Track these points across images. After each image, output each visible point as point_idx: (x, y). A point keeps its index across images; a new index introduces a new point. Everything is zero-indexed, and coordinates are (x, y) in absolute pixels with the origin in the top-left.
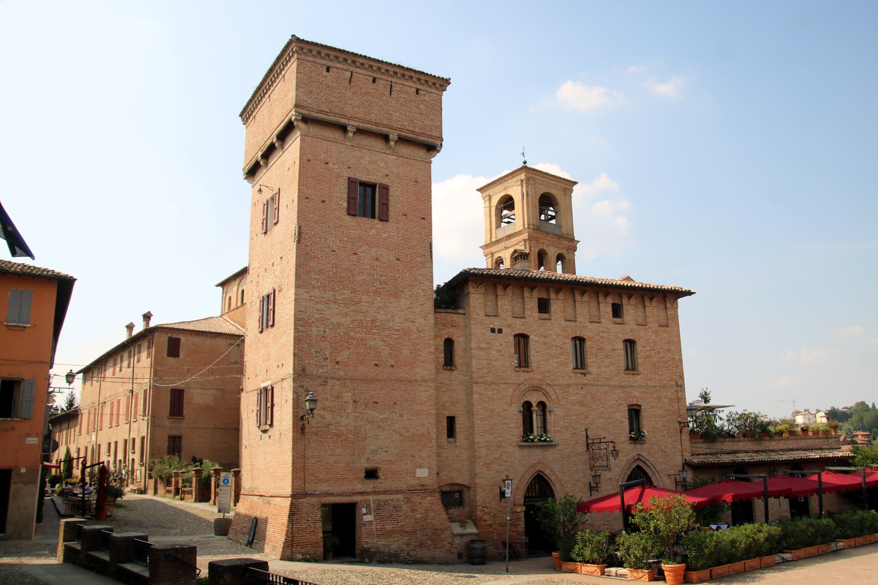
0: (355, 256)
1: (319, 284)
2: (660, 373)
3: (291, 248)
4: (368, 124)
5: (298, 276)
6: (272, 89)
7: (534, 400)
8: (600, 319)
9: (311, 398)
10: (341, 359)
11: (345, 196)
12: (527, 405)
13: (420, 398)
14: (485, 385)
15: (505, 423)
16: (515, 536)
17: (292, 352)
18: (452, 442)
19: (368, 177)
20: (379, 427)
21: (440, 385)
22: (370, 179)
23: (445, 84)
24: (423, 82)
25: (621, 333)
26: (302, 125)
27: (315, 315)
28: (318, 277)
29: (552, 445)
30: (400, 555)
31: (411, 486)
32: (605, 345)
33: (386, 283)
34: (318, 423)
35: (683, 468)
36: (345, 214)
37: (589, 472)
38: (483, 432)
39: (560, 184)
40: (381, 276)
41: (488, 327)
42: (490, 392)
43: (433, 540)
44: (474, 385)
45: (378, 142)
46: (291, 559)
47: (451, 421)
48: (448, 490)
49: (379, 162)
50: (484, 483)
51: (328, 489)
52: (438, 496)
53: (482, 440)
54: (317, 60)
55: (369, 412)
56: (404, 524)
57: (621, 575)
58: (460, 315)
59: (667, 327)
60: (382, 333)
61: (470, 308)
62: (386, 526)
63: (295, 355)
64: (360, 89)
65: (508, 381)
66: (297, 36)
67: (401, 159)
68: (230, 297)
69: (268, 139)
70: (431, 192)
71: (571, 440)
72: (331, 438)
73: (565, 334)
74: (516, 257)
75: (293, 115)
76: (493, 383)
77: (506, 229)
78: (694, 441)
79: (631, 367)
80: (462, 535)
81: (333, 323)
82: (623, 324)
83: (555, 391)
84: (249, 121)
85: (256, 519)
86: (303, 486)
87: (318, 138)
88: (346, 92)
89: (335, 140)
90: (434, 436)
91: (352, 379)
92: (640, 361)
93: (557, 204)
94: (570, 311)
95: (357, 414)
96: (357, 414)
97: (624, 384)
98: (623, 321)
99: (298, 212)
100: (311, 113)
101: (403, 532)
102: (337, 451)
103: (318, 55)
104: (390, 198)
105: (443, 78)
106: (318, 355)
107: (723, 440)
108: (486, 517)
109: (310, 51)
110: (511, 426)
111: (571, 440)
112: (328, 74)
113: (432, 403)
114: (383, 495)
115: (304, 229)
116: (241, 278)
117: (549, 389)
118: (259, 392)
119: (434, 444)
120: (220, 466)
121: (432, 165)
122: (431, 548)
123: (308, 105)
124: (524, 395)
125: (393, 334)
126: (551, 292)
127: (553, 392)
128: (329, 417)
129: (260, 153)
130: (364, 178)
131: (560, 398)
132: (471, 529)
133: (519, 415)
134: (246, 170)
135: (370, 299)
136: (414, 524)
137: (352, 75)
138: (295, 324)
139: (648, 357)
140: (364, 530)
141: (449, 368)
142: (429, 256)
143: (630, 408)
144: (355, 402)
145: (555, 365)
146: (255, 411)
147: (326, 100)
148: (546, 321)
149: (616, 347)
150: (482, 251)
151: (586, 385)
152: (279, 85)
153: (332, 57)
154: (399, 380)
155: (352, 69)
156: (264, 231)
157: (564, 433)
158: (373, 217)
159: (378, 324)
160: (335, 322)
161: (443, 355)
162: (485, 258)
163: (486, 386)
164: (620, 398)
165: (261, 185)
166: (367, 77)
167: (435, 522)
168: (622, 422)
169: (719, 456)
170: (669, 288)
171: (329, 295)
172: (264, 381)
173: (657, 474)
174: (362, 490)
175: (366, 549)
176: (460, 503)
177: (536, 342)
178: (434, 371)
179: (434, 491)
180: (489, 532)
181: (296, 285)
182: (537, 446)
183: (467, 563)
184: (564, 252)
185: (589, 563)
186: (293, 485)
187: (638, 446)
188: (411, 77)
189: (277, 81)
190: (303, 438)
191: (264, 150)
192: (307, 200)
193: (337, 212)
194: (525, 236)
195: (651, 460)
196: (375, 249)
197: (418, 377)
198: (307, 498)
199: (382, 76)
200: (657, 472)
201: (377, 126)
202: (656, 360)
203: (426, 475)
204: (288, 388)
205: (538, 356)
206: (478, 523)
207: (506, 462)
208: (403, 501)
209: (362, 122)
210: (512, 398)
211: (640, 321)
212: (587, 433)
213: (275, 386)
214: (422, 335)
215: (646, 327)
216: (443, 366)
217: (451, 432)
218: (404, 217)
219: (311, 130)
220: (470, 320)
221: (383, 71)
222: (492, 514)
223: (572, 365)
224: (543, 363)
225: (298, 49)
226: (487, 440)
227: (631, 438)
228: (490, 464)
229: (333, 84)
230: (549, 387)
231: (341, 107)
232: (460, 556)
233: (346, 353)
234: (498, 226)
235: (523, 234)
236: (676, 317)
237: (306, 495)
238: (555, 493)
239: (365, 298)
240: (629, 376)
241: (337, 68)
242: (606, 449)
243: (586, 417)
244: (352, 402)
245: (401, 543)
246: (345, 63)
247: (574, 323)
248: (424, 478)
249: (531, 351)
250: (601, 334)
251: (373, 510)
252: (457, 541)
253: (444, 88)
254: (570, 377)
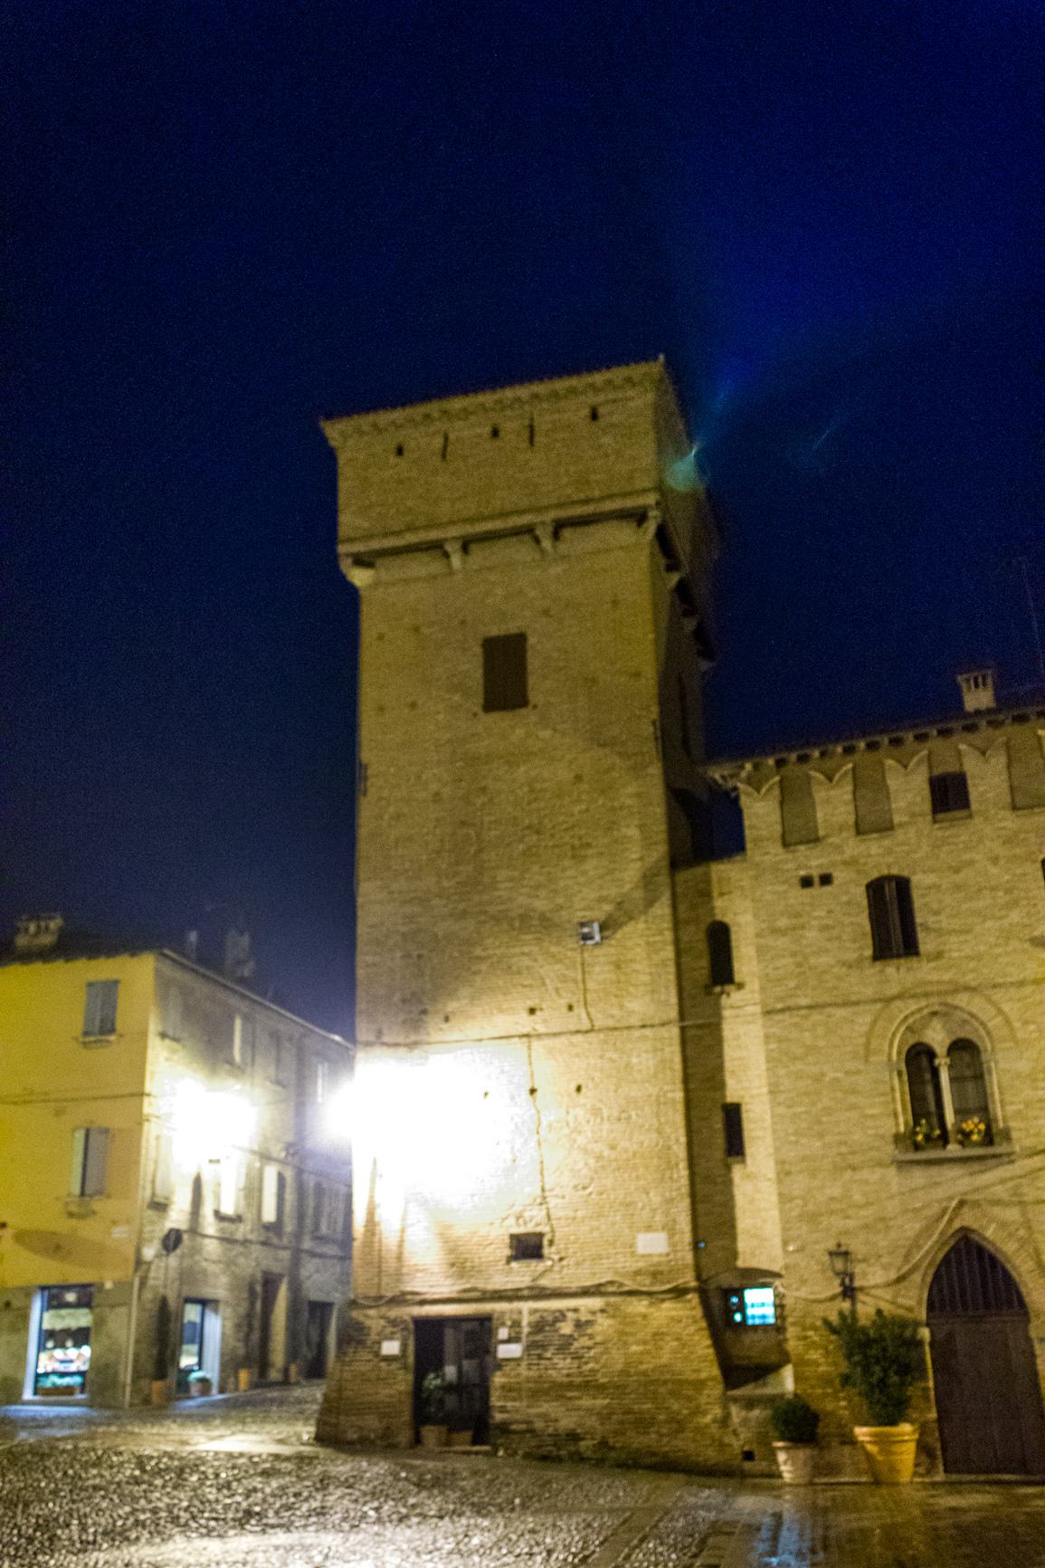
12: (919, 1060)
15: (853, 1107)
42: (807, 1034)
110: (869, 1112)
112: (398, 460)
127: (993, 1012)
131: (1017, 1025)
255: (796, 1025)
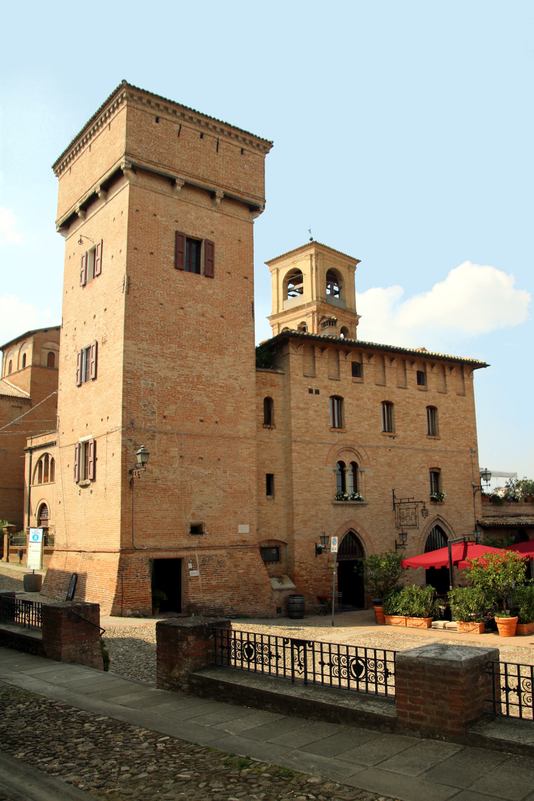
0: (181, 310)
1: (148, 336)
2: (458, 439)
3: (118, 299)
4: (196, 178)
5: (127, 328)
6: (93, 138)
7: (347, 460)
8: (406, 385)
9: (143, 452)
10: (168, 413)
11: (173, 249)
12: (342, 464)
13: (242, 455)
14: (303, 444)
15: (321, 482)
16: (329, 591)
17: (121, 404)
18: (270, 499)
19: (194, 232)
20: (204, 483)
21: (260, 443)
22: (196, 234)
23: (268, 147)
24: (248, 142)
25: (425, 400)
26: (131, 174)
27: (143, 368)
28: (147, 330)
29: (363, 504)
30: (224, 610)
31: (233, 542)
32: (411, 410)
33: (211, 340)
34: (146, 477)
35: (476, 529)
36: (173, 267)
37: (395, 530)
38: (301, 490)
39: (345, 261)
40: (207, 332)
41: (307, 388)
43: (254, 595)
44: (293, 443)
45: (204, 198)
46: (121, 615)
47: (270, 478)
48: (266, 546)
49: (205, 218)
50: (301, 539)
51: (155, 544)
52: (258, 551)
53: (300, 497)
54: (146, 109)
55: (195, 467)
56: (227, 579)
57: (449, 628)
58: (279, 375)
59: (464, 395)
60: (208, 389)
61: (289, 369)
62: (211, 582)
63: (123, 407)
64: (189, 143)
65: (324, 441)
66: (129, 82)
67: (226, 217)
68: (11, 361)
69: (89, 190)
70: (253, 252)
71: (380, 500)
72: (159, 493)
73: (375, 398)
74: (324, 323)
75: (122, 163)
76: (310, 442)
77: (292, 302)
78: (484, 504)
79: (433, 432)
80: (281, 590)
81: (161, 377)
82: (426, 391)
83: (366, 453)
84: (63, 173)
85: (75, 574)
86: (131, 541)
87: (146, 189)
88: (175, 144)
89: (163, 193)
90: (255, 493)
91: (178, 434)
92: (440, 427)
93: (342, 280)
94: (380, 376)
95: (184, 469)
96: (184, 469)
97: (426, 448)
98: (426, 388)
99: (127, 262)
100: (141, 162)
101: (227, 587)
102: (165, 506)
103: (148, 104)
104: (215, 255)
105: (266, 140)
106: (146, 408)
107: (508, 503)
108: (303, 573)
109: (140, 99)
110: (326, 484)
111: (380, 500)
112: (157, 124)
113: (253, 460)
114: (207, 551)
115: (133, 280)
116: (23, 342)
117: (361, 451)
118: (77, 446)
119: (254, 500)
120: (9, 523)
121: (254, 225)
122: (253, 603)
123: (138, 154)
124: (338, 455)
125: (218, 391)
126: (363, 356)
127: (364, 454)
128: (156, 472)
129: (78, 205)
130: (190, 233)
131: (371, 459)
132: (289, 585)
133: (333, 474)
134: (61, 222)
135: (196, 355)
136: (237, 579)
137: (180, 128)
138: (124, 376)
139: (447, 424)
140: (191, 585)
141: (269, 426)
142: (251, 315)
143: (431, 471)
144: (181, 457)
145: (367, 427)
146: (72, 466)
147: (155, 150)
148: (359, 385)
149: (420, 412)
150: (268, 321)
151: (393, 447)
152: (103, 134)
153: (161, 107)
154: (222, 436)
155: (181, 122)
156: (83, 283)
157: (374, 492)
158: (198, 272)
159: (204, 380)
160: (162, 376)
161: (263, 414)
162: (272, 328)
163: (304, 445)
164: (423, 461)
165: (81, 236)
166: (195, 131)
167: (256, 577)
168: (424, 484)
169: (505, 518)
170: (468, 359)
171: (157, 348)
172: (83, 436)
173: (453, 534)
174: (188, 546)
175: (193, 604)
176: (277, 559)
177: (349, 404)
178: (255, 429)
179: (254, 547)
180: (305, 587)
181: (125, 336)
182: (349, 504)
183: (285, 617)
184: (347, 325)
185: (416, 617)
186: (122, 540)
187: (438, 507)
188: (237, 137)
189: (101, 130)
190: (131, 492)
191: (84, 201)
192: (135, 251)
193: (165, 265)
194: (314, 308)
195: (449, 520)
196: (201, 305)
197: (241, 434)
198: (135, 554)
199: (209, 132)
200: (454, 532)
201: (205, 182)
202: (454, 426)
203: (247, 531)
204: (116, 442)
205: (351, 417)
206: (296, 578)
207: (321, 519)
208: (226, 556)
209: (190, 177)
210: (327, 458)
211: (441, 388)
212: (393, 493)
213: (97, 440)
214: (244, 393)
215: (446, 395)
216: (263, 424)
217: (270, 490)
218: (227, 274)
219: (140, 180)
220: (290, 380)
221: (210, 127)
222: (308, 570)
223: (382, 428)
224: (355, 425)
225: (128, 95)
226: (305, 498)
227: (433, 499)
228: (307, 521)
229: (162, 135)
230: (361, 448)
231: (170, 159)
232: (279, 610)
233: (173, 407)
234: (285, 298)
235: (312, 306)
236: (471, 387)
237: (134, 550)
238: (365, 550)
239: (191, 353)
240: (431, 440)
241: (166, 119)
242: (415, 508)
243: (394, 478)
244: (178, 457)
245: (225, 598)
246: (173, 115)
247: (383, 388)
248: (246, 534)
249: (345, 413)
250: (407, 400)
251: (198, 565)
252: (276, 595)
253: (267, 150)
254: (380, 439)
255: (303, 447)
